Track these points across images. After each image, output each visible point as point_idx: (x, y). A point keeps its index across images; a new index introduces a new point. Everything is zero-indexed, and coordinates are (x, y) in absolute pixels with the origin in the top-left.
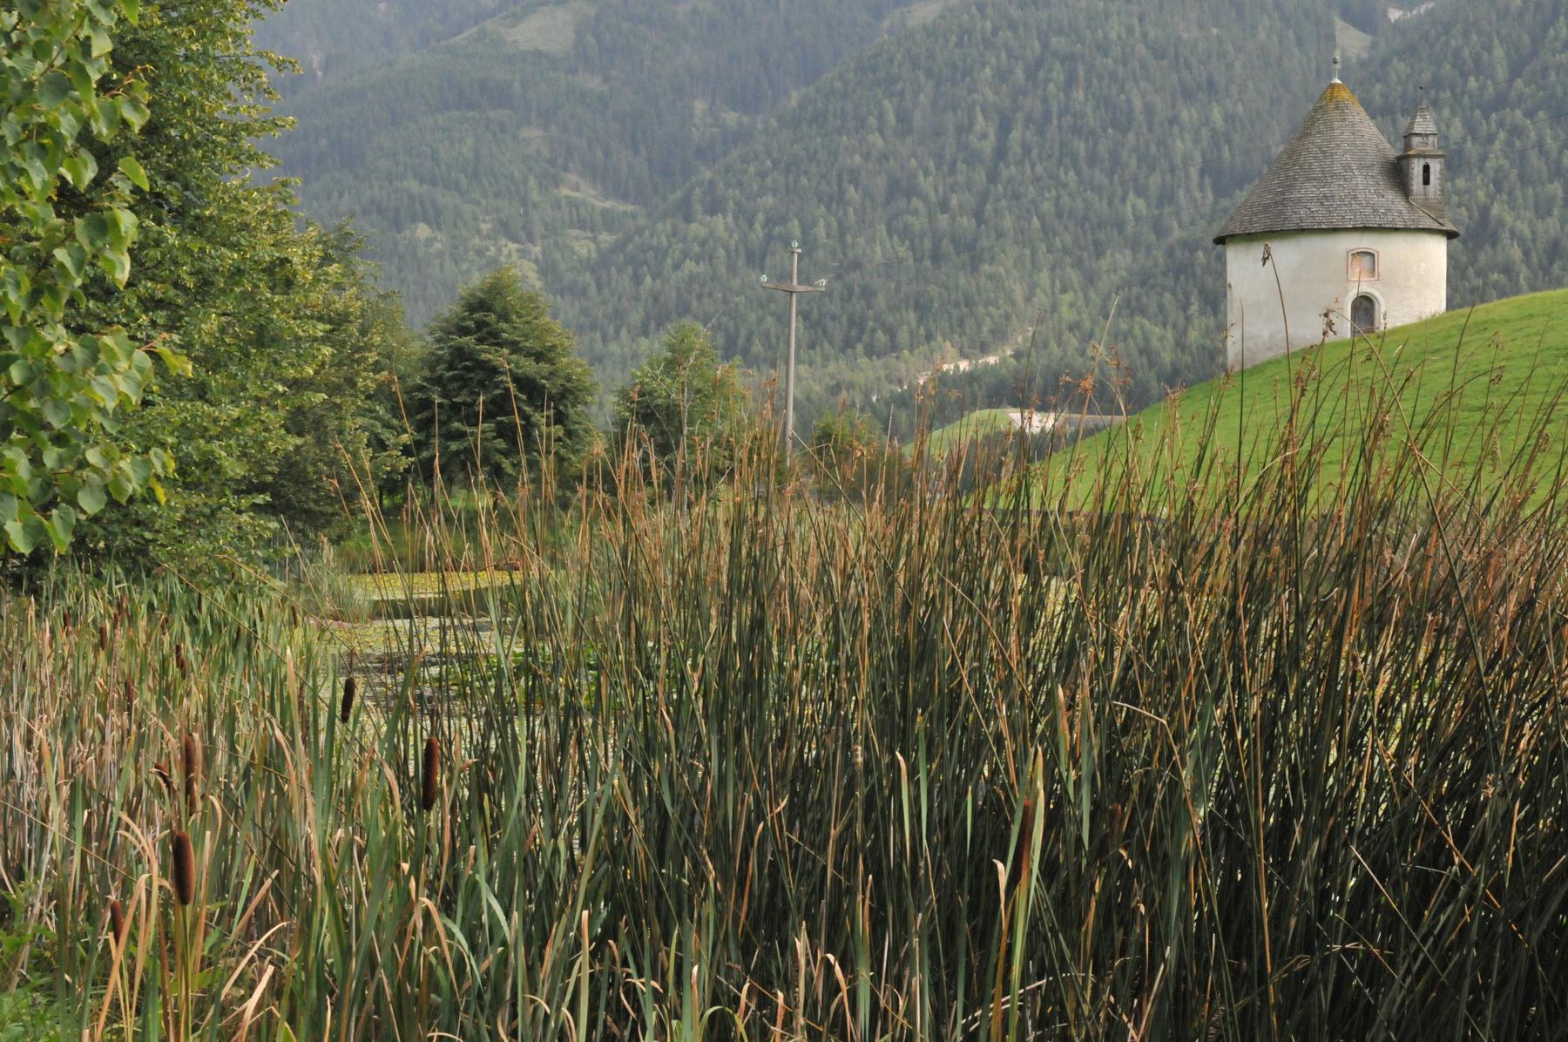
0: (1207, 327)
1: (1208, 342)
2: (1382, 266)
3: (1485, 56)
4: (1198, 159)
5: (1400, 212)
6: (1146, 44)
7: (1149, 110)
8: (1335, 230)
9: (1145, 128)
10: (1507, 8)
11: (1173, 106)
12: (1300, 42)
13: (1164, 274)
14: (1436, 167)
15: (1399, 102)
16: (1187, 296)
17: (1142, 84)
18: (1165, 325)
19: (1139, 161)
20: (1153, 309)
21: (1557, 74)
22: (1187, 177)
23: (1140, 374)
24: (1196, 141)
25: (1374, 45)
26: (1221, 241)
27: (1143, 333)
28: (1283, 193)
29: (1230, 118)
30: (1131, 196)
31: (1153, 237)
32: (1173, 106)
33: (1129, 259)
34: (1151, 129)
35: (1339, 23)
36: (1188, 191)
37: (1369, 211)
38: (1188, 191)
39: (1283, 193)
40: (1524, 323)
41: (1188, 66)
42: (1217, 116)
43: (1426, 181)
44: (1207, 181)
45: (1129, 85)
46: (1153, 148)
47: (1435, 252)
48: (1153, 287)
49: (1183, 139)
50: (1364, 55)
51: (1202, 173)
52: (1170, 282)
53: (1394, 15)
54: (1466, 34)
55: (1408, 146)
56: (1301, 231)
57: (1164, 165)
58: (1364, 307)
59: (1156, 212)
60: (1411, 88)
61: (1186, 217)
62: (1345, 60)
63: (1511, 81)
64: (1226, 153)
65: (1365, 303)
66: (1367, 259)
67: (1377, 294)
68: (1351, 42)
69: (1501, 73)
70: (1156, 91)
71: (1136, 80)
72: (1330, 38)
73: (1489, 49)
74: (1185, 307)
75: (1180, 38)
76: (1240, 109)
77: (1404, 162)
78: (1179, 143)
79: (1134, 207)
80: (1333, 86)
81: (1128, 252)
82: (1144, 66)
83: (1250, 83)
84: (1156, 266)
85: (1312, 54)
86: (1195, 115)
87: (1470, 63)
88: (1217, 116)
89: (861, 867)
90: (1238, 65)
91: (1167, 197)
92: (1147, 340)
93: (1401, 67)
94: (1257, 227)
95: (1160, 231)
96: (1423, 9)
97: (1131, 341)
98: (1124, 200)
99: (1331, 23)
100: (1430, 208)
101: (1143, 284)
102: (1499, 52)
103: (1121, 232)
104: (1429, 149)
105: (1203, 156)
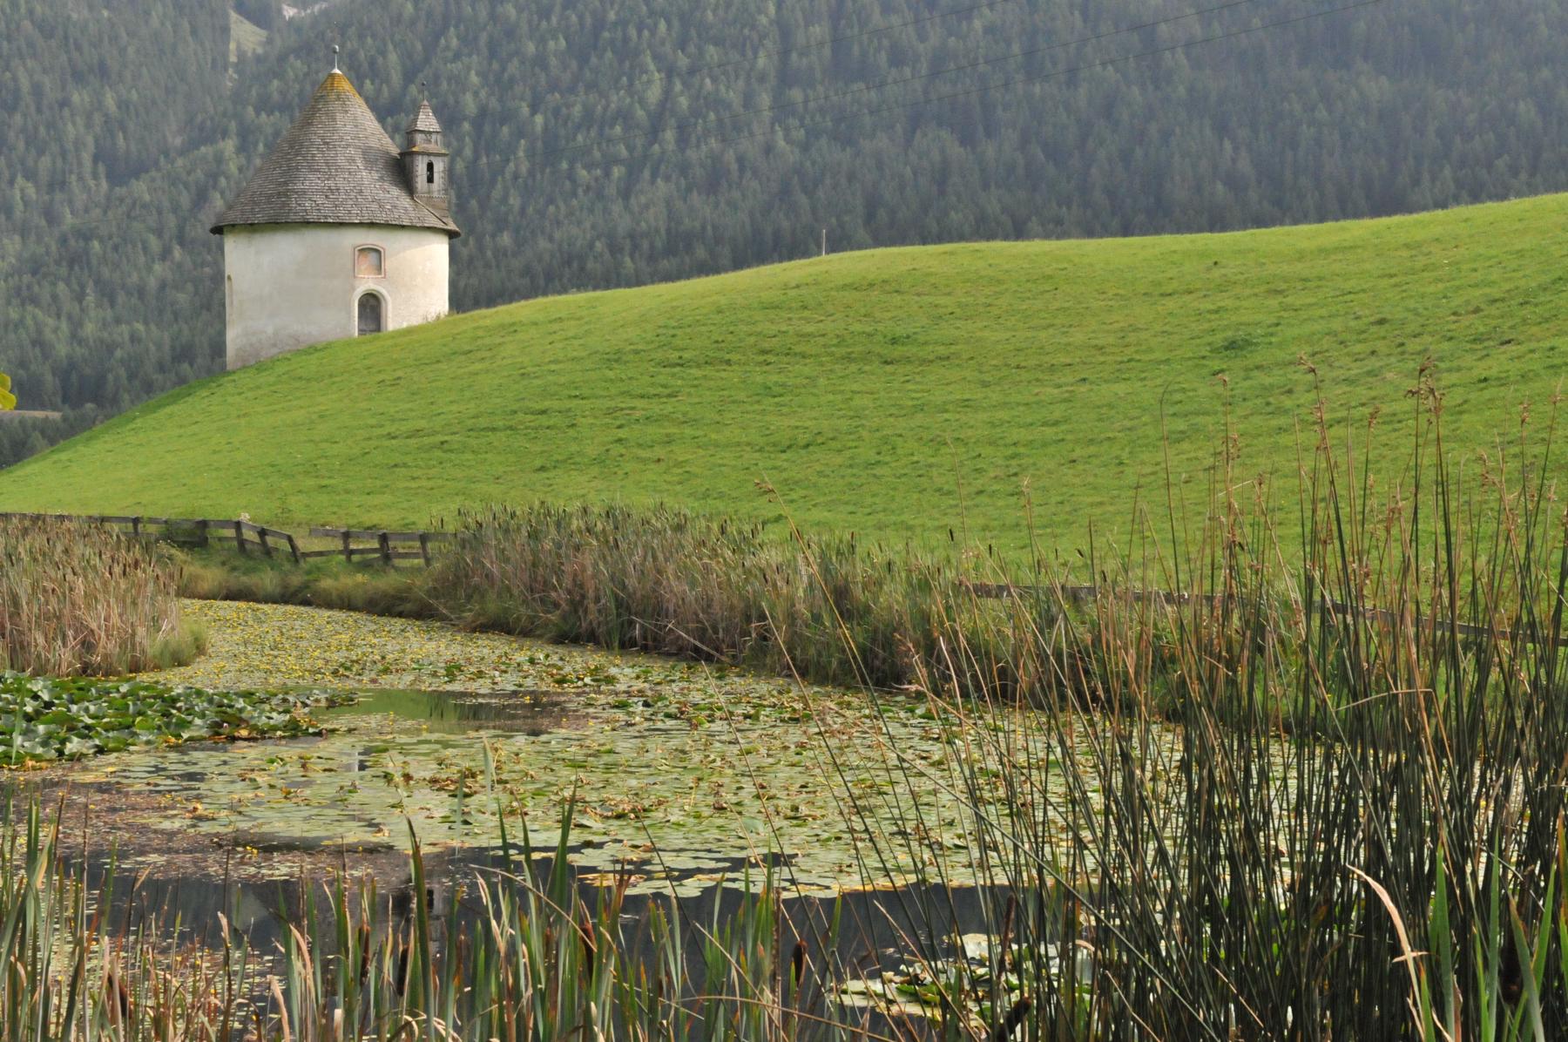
0: (104, 319)
1: (106, 335)
2: (388, 264)
3: (380, 60)
4: (90, 140)
5: (406, 209)
6: (33, 22)
7: (37, 91)
8: (342, 225)
9: (33, 109)
10: (400, 15)
11: (63, 88)
12: (194, 32)
13: (58, 263)
14: (439, 166)
15: (296, 100)
16: (83, 287)
17: (29, 63)
18: (58, 316)
19: (27, 144)
20: (45, 297)
21: (449, 84)
22: (80, 164)
23: (33, 367)
24: (89, 125)
25: (270, 41)
26: (218, 230)
27: (36, 324)
28: (286, 183)
29: (123, 105)
30: (20, 180)
31: (43, 223)
32: (63, 88)
33: (18, 247)
34: (39, 110)
35: (233, 15)
36: (81, 178)
37: (375, 206)
38: (81, 178)
39: (286, 183)
40: (556, 326)
41: (78, 48)
42: (110, 101)
43: (430, 180)
44: (101, 168)
45: (16, 62)
46: (42, 130)
47: (439, 249)
48: (45, 276)
49: (74, 123)
50: (260, 51)
51: (96, 159)
52: (64, 271)
53: (289, 12)
54: (361, 37)
55: (411, 143)
56: (307, 224)
57: (55, 148)
58: (371, 306)
59: (46, 198)
60: (308, 87)
61: (79, 205)
62: (241, 55)
63: (405, 87)
64: (121, 141)
65: (372, 301)
66: (373, 256)
67: (384, 292)
68: (245, 36)
69: (396, 78)
70: (45, 71)
71: (22, 57)
72: (225, 30)
73: (383, 53)
74: (80, 297)
75: (69, 18)
76: (134, 96)
77: (408, 159)
78: (70, 127)
79: (22, 190)
80: (332, 76)
81: (17, 238)
82: (31, 45)
83: (144, 70)
84: (48, 253)
85: (208, 45)
86: (87, 99)
87: (366, 65)
88: (110, 101)
89: (1350, 951)
90: (131, 50)
91: (57, 183)
92: (39, 332)
93: (297, 65)
94: (259, 218)
95: (51, 217)
96: (317, 8)
97: (22, 332)
98: (11, 182)
99: (226, 16)
100: (434, 206)
101: (34, 273)
102: (393, 57)
103: (9, 218)
104: (432, 148)
105: (96, 141)
